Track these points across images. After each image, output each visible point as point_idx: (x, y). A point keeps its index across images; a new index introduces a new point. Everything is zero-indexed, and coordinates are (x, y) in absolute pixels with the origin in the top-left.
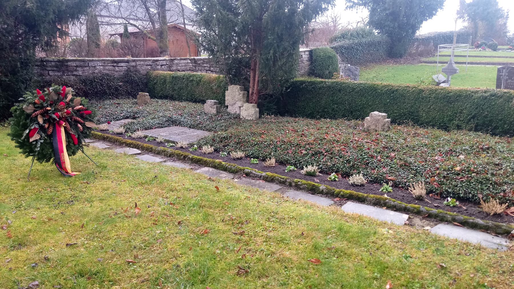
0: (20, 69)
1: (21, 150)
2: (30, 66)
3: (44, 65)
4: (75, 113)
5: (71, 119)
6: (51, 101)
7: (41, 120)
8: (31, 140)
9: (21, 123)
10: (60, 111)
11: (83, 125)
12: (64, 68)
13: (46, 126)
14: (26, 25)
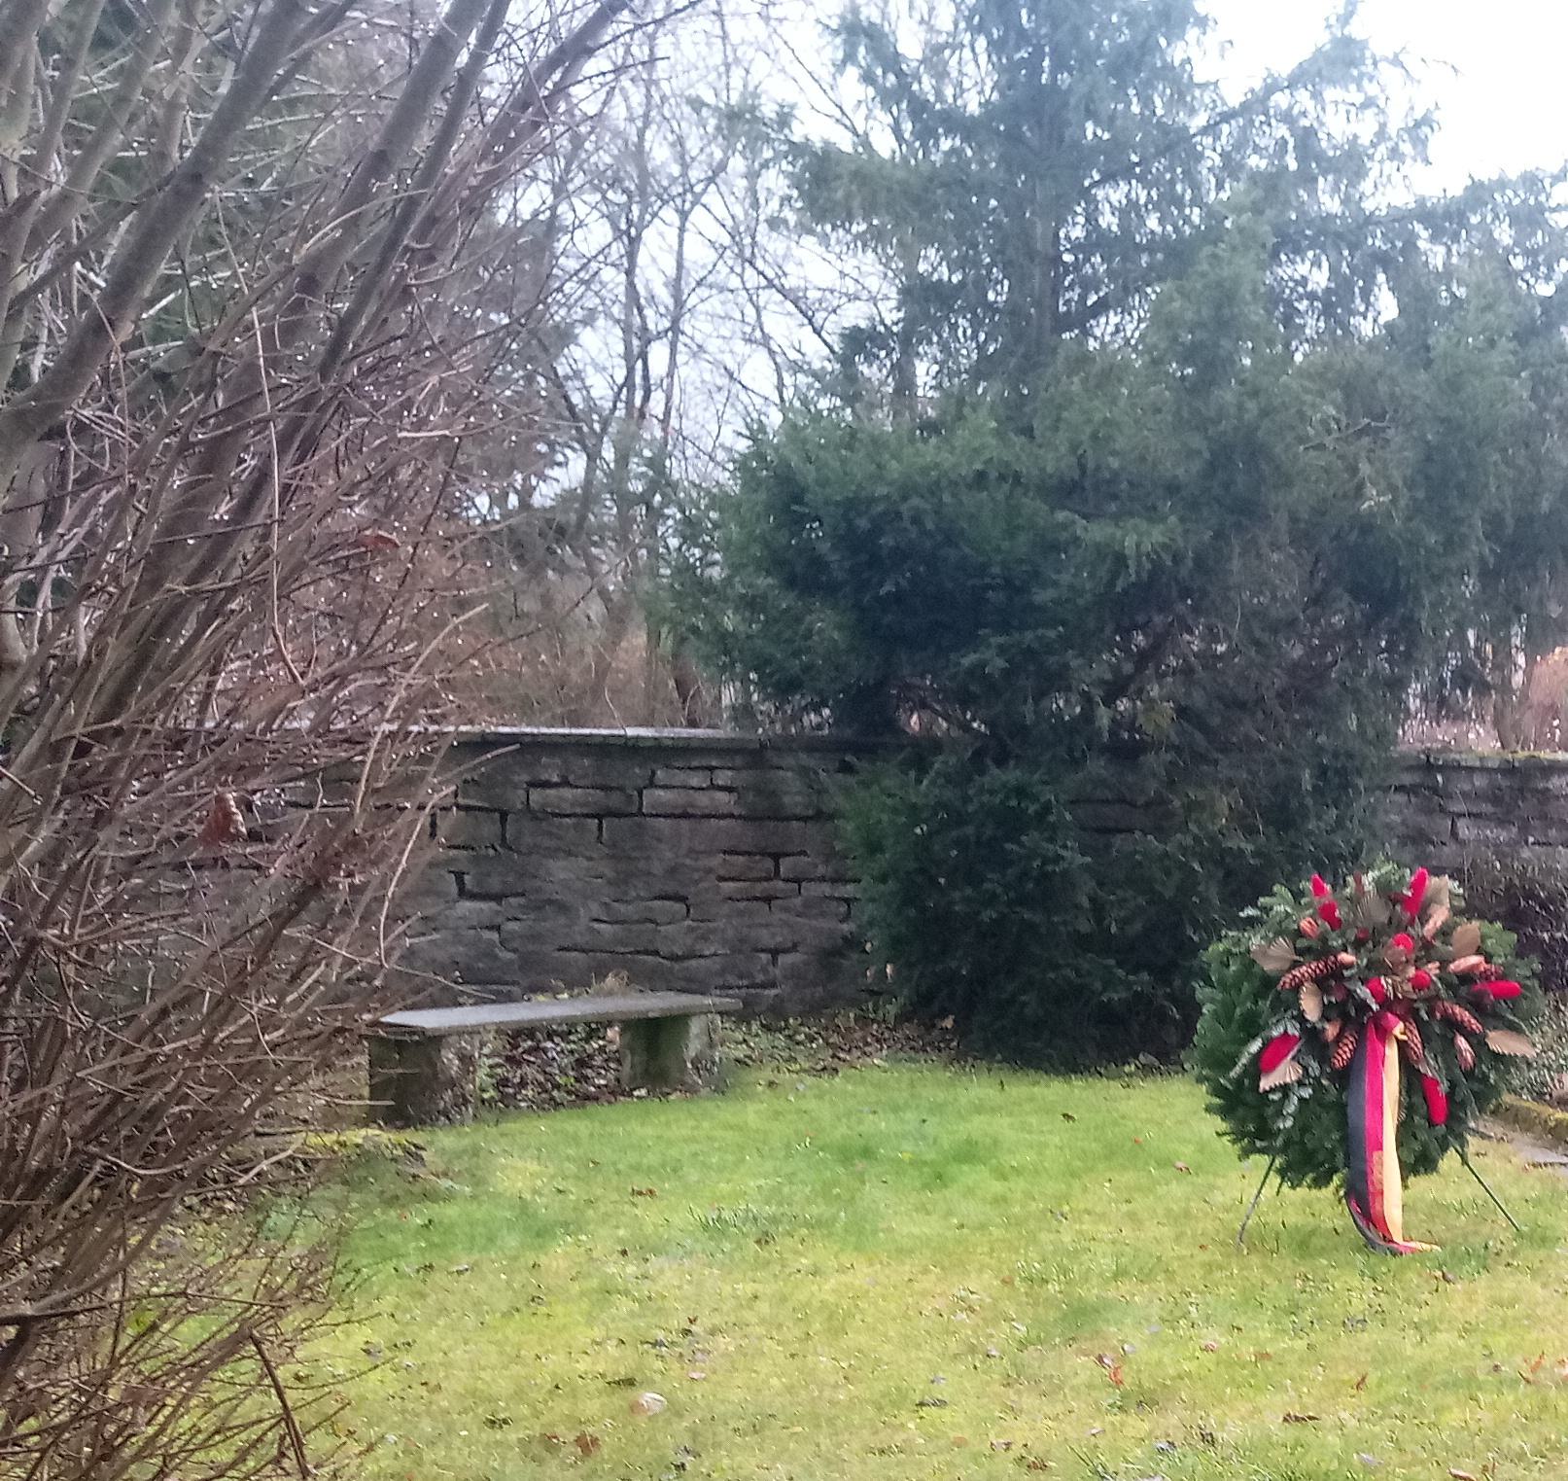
0: (1309, 802)
1: (1223, 1126)
2: (1356, 787)
3: (1435, 790)
4: (1448, 986)
5: (1431, 1013)
6: (1365, 931)
7: (1310, 1006)
8: (1265, 1084)
9: (1238, 1011)
10: (1390, 972)
11: (1478, 1043)
12: (1526, 807)
13: (1331, 1031)
14: (1357, 592)
